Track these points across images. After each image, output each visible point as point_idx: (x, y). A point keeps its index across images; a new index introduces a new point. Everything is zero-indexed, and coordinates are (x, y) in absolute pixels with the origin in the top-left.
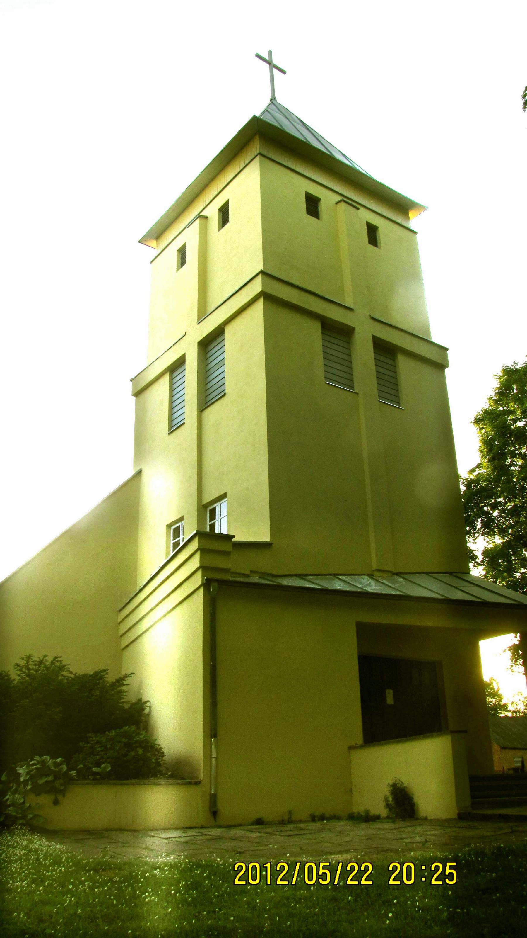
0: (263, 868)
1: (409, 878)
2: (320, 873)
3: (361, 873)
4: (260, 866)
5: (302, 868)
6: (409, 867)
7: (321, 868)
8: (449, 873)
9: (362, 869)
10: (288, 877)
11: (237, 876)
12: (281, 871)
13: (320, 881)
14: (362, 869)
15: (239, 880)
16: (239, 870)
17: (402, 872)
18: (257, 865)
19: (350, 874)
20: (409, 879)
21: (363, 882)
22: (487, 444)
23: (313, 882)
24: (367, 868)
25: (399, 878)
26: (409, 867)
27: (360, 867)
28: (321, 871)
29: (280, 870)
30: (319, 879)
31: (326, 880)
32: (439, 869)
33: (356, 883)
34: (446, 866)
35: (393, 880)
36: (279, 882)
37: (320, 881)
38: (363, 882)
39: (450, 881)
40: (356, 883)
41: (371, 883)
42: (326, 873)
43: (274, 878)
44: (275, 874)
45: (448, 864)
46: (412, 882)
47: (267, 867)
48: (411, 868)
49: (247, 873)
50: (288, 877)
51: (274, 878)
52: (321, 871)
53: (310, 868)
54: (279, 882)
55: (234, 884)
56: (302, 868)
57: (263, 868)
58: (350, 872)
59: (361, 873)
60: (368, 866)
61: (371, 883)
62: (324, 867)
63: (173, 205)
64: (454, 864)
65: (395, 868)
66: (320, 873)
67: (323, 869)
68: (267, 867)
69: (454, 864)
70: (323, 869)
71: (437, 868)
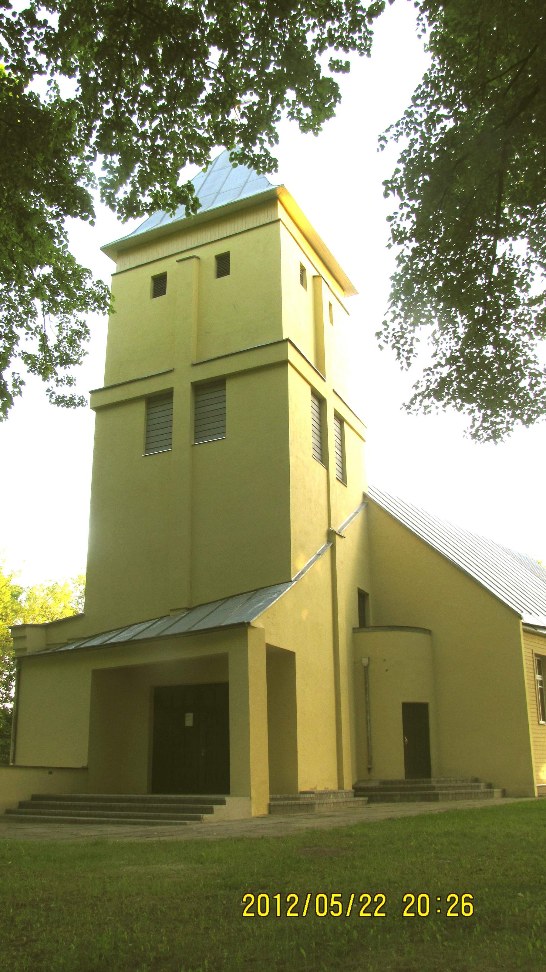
0: (273, 902)
1: (424, 910)
2: (332, 905)
3: (374, 905)
4: (269, 897)
5: (312, 901)
6: (423, 899)
7: (332, 899)
8: (334, 905)
9: (376, 900)
10: (298, 909)
11: (449, 908)
12: (408, 902)
13: (332, 912)
14: (376, 900)
15: (364, 912)
16: (364, 903)
17: (255, 904)
18: (267, 897)
19: (290, 906)
20: (263, 911)
21: (376, 914)
22: (5, 394)
23: (325, 913)
24: (380, 899)
25: (413, 909)
26: (423, 899)
27: (373, 898)
28: (333, 903)
29: (406, 902)
30: (330, 910)
31: (338, 912)
32: (455, 900)
33: (369, 915)
34: (331, 897)
35: (291, 912)
36: (289, 914)
37: (332, 912)
38: (376, 914)
39: (335, 913)
40: (369, 915)
41: (384, 915)
42: (337, 905)
43: (284, 910)
44: (285, 906)
45: (334, 896)
46: (427, 914)
47: (276, 899)
48: (324, 899)
49: (255, 904)
50: (298, 909)
51: (284, 910)
52: (333, 903)
53: (322, 899)
54: (289, 914)
55: (447, 916)
56: (312, 901)
57: (273, 902)
58: (362, 904)
59: (374, 905)
60: (410, 897)
61: (384, 915)
62: (366, 899)
63: (109, 256)
64: (340, 895)
65: (409, 899)
66: (332, 905)
67: (335, 900)
68: (276, 899)
69: (340, 895)
70: (335, 900)
71: (453, 899)
